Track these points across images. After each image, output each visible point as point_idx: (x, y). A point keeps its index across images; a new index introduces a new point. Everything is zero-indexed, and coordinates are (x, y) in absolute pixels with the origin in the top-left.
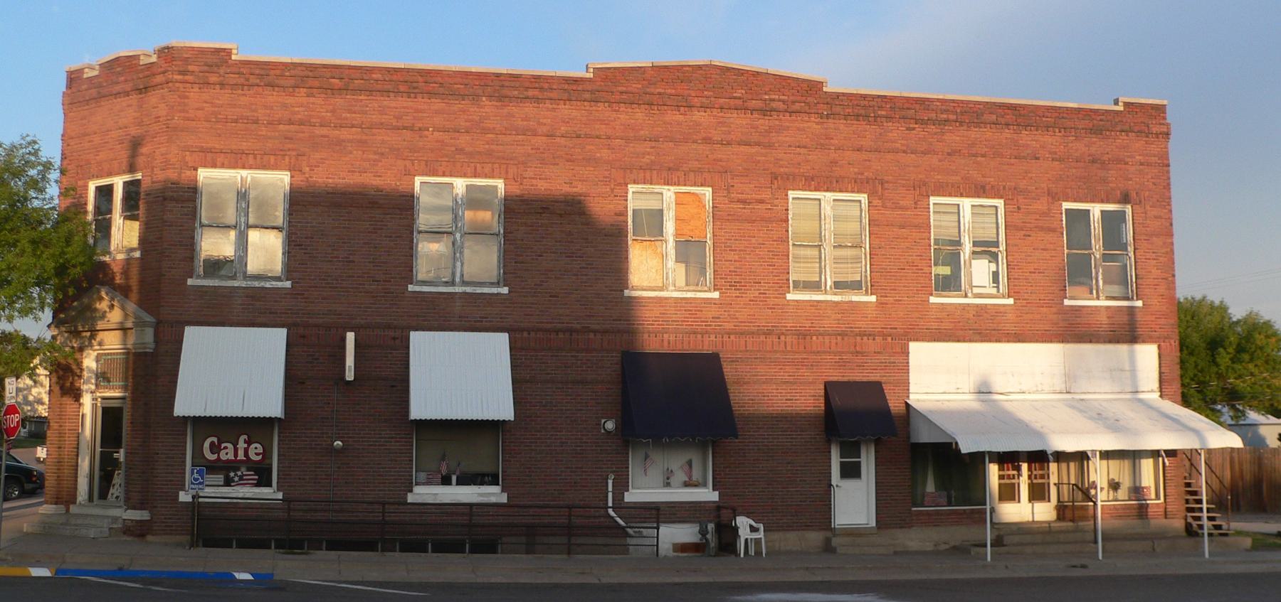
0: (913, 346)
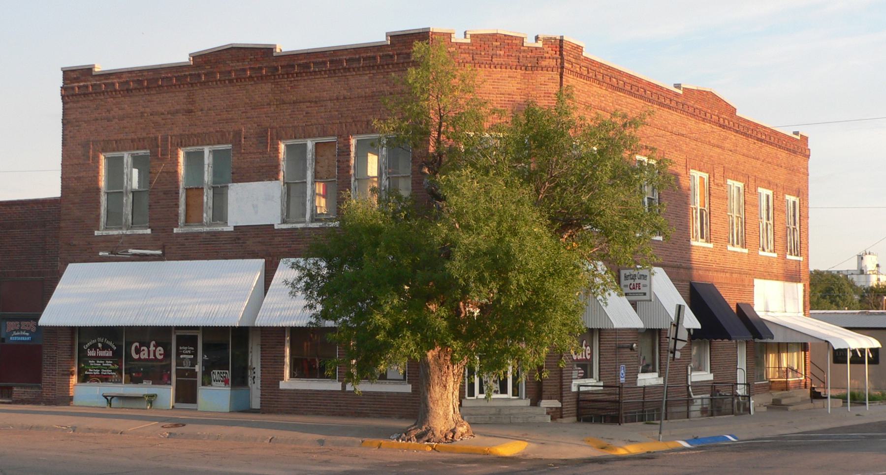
0: (757, 282)
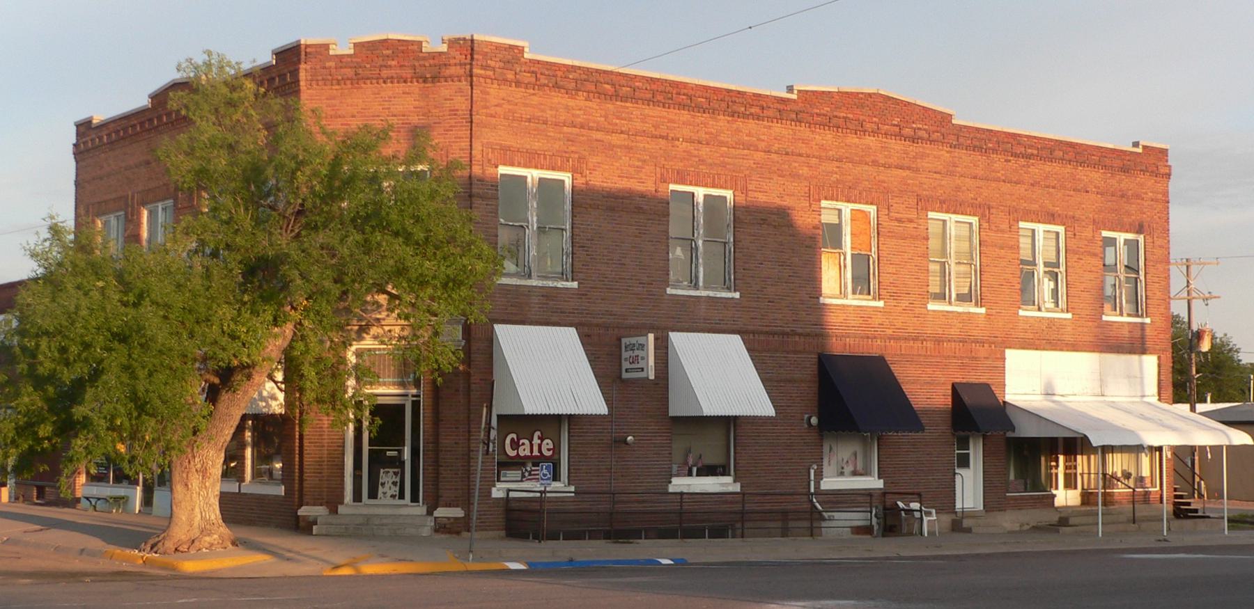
0: (1009, 353)
